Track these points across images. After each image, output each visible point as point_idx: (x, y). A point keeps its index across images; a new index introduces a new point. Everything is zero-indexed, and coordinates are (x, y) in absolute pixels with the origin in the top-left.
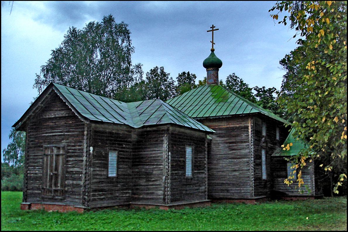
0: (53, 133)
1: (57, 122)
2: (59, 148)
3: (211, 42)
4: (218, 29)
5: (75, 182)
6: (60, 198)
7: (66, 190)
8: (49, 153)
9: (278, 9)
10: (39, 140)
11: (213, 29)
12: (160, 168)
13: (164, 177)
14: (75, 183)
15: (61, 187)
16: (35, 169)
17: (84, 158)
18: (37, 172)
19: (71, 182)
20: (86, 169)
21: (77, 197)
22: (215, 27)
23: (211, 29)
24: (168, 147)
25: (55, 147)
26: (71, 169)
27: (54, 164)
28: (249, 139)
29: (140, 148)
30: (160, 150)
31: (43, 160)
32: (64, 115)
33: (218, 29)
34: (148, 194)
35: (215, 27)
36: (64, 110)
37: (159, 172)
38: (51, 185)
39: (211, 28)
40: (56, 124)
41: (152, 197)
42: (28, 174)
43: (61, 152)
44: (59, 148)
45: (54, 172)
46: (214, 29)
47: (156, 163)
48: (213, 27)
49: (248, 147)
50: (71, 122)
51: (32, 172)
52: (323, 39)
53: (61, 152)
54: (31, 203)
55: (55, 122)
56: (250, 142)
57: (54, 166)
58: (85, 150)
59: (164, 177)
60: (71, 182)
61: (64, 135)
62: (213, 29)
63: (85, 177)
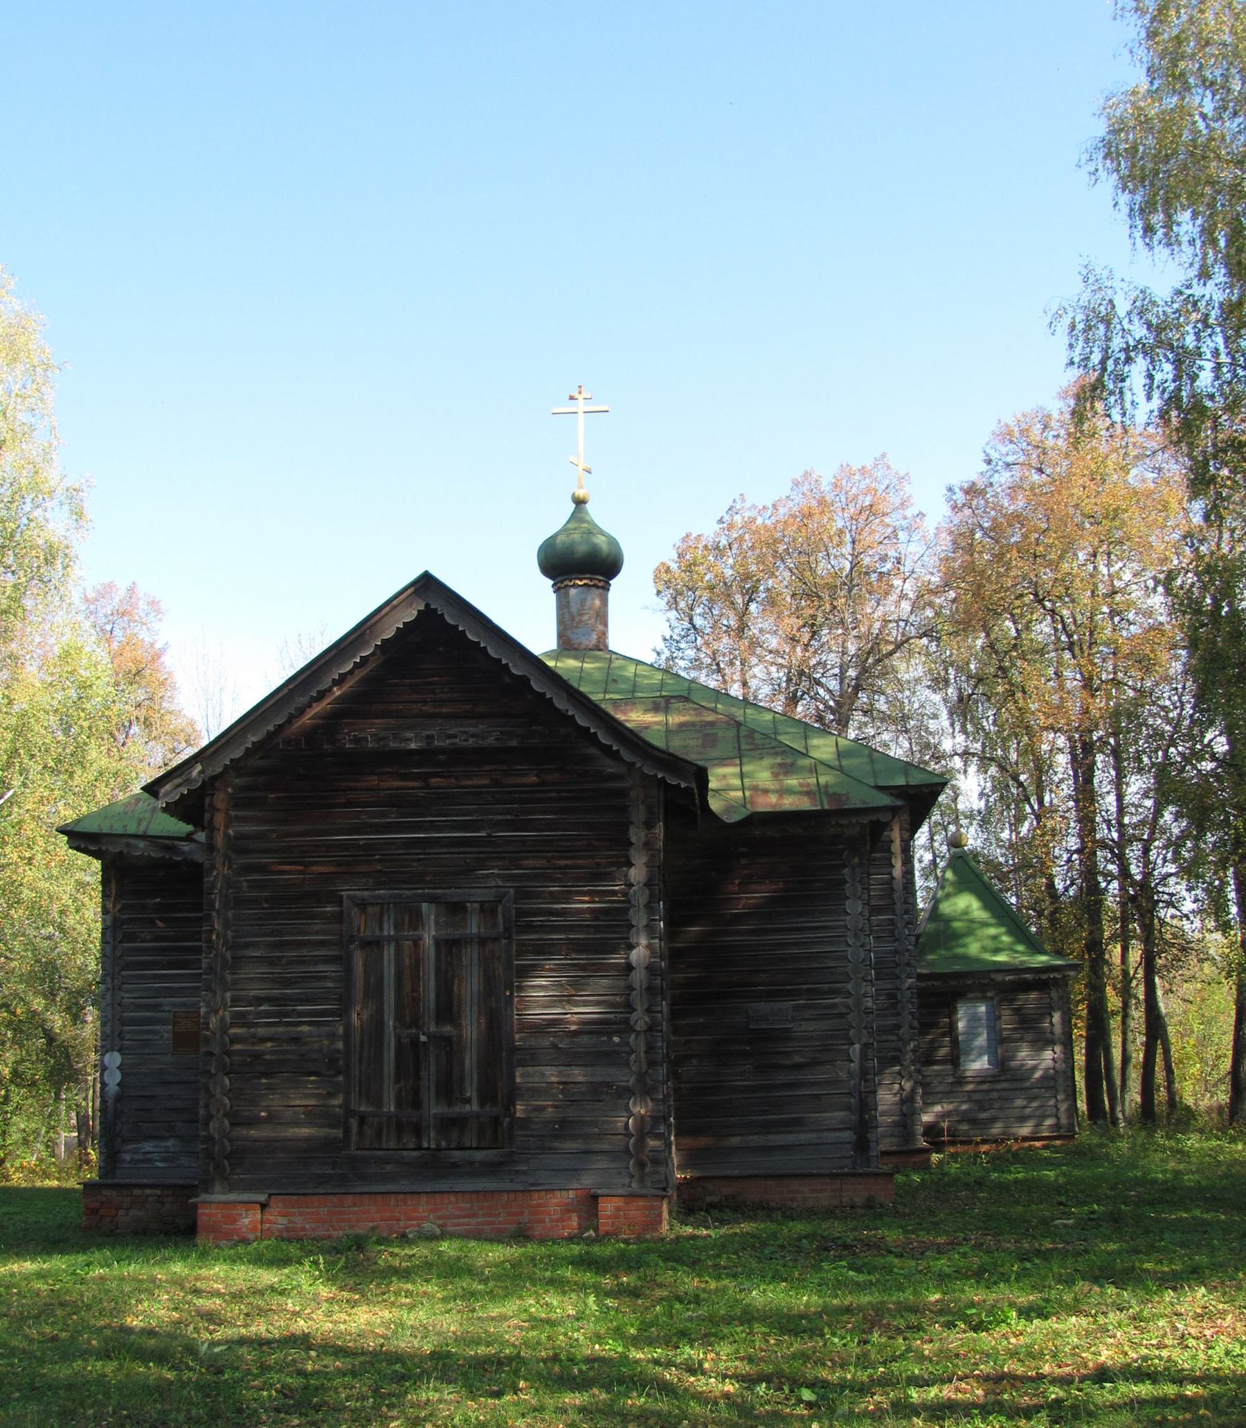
0: (426, 831)
1: (436, 775)
6: (480, 1155)
10: (307, 865)
12: (834, 1006)
15: (482, 1104)
16: (286, 1015)
18: (305, 1028)
20: (649, 1011)
25: (433, 899)
27: (432, 984)
28: (896, 895)
29: (597, 929)
30: (826, 928)
31: (349, 970)
32: (490, 741)
34: (769, 1127)
36: (480, 717)
37: (826, 1025)
38: (416, 1091)
40: (428, 787)
41: (789, 1138)
43: (474, 927)
44: (457, 909)
45: (433, 1029)
47: (806, 986)
50: (533, 779)
51: (262, 1031)
52: (29, 509)
53: (474, 927)
55: (425, 777)
57: (432, 996)
59: (857, 1046)
61: (488, 841)
63: (650, 1048)
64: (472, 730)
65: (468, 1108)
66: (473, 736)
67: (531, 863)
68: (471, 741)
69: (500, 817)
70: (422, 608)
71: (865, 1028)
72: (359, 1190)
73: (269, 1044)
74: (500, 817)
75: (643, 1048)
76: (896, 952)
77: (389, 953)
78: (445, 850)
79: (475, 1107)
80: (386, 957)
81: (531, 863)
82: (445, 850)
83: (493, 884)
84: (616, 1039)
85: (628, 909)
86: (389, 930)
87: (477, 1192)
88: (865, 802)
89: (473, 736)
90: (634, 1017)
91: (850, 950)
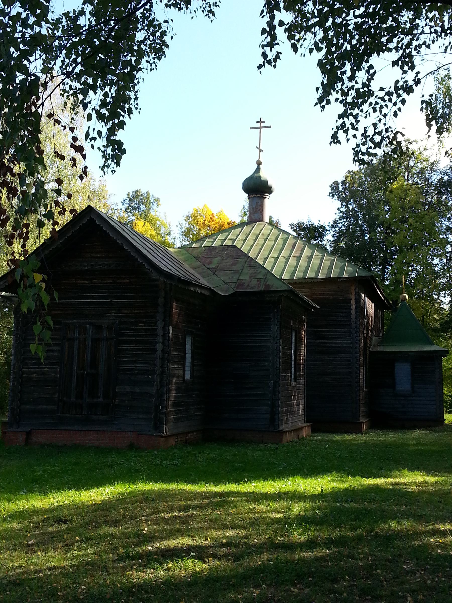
2: (99, 328)
3: (257, 147)
4: (270, 127)
5: (137, 389)
7: (116, 403)
8: (76, 335)
9: (52, 19)
11: (261, 124)
13: (272, 382)
14: (137, 391)
17: (159, 347)
18: (46, 369)
19: (128, 389)
21: (141, 416)
22: (264, 122)
23: (258, 125)
24: (279, 331)
26: (129, 366)
28: (352, 321)
33: (270, 127)
35: (264, 122)
39: (257, 122)
42: (23, 374)
43: (105, 334)
46: (263, 125)
48: (260, 122)
49: (350, 335)
50: (127, 281)
54: (31, 429)
56: (353, 325)
58: (160, 332)
59: (272, 382)
60: (128, 389)
62: (261, 124)
64: (106, 263)
65: (99, 400)
66: (107, 265)
67: (125, 311)
68: (106, 266)
69: (115, 294)
70: (89, 218)
71: (276, 375)
72: (62, 428)
73: (35, 375)
74: (115, 294)
75: (159, 381)
76: (351, 343)
77: (76, 343)
78: (96, 306)
79: (102, 400)
80: (75, 344)
81: (125, 311)
82: (96, 306)
83: (112, 319)
84: (150, 377)
85: (157, 329)
86: (76, 335)
87: (100, 431)
88: (277, 288)
89: (107, 265)
90: (156, 368)
91: (271, 345)
